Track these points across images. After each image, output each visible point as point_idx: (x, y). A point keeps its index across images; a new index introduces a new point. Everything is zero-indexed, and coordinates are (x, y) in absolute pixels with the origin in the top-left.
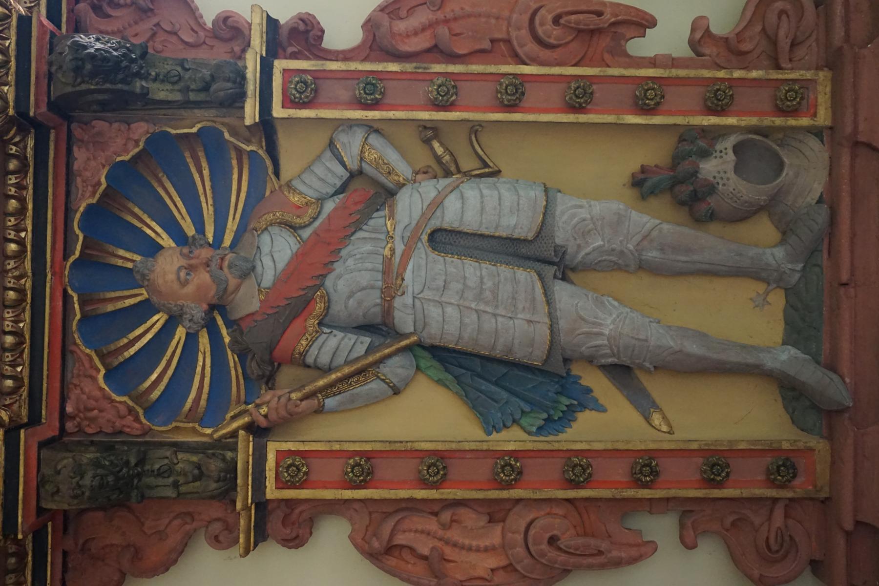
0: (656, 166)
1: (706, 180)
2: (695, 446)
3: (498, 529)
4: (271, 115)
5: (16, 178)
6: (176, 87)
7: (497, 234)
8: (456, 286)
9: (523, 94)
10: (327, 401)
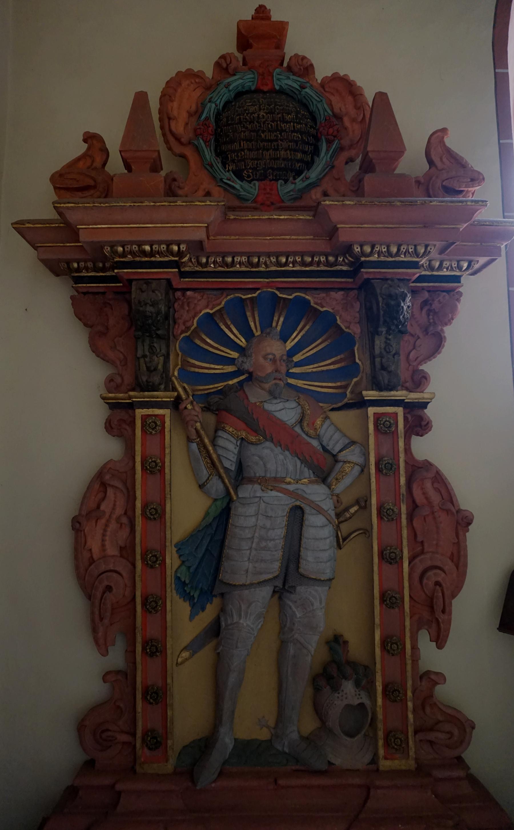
0: (348, 651)
1: (341, 685)
2: (169, 681)
3: (116, 553)
4: (369, 406)
5: (324, 261)
6: (383, 351)
7: (302, 549)
8: (268, 524)
9: (391, 563)
10: (195, 444)
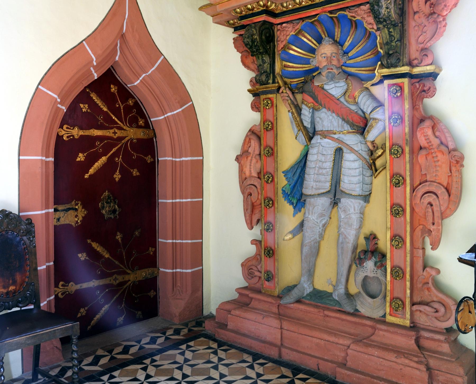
3: (256, 175)
8: (323, 158)
